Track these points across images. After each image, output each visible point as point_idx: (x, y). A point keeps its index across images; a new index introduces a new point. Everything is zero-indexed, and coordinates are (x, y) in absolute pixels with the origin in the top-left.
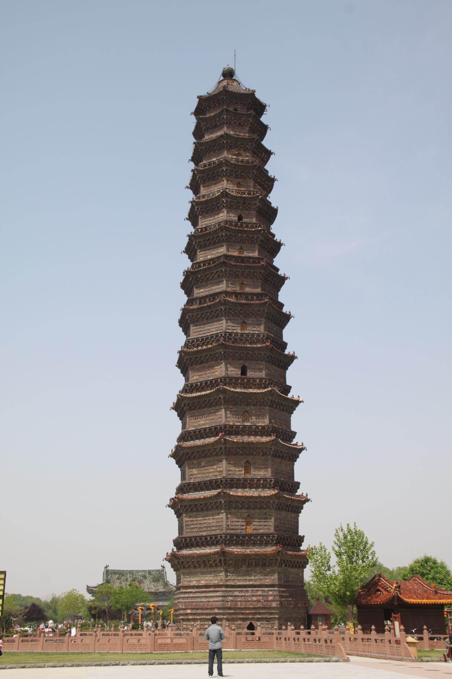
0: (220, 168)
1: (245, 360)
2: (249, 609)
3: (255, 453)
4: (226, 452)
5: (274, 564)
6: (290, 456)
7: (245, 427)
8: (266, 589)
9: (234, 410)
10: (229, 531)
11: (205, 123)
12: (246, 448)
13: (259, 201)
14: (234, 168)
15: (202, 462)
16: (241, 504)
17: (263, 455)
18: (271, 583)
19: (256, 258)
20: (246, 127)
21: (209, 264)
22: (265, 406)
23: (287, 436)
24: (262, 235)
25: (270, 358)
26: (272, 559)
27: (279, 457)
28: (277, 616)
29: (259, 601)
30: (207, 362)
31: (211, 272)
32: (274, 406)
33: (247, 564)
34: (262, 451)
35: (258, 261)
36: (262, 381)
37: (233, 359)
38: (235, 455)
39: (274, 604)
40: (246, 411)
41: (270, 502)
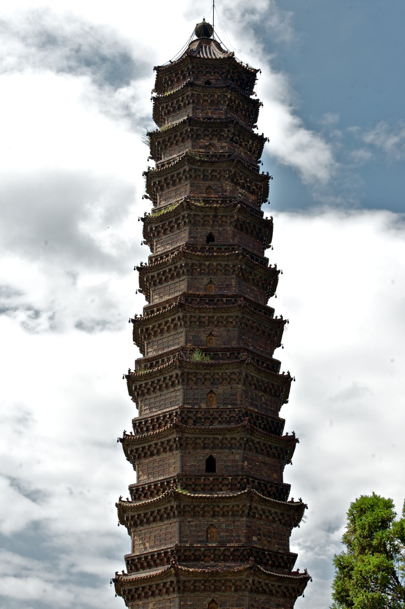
0: (181, 167)
1: (213, 448)
3: (223, 588)
4: (179, 588)
6: (285, 590)
9: (193, 524)
12: (210, 581)
15: (149, 603)
17: (236, 590)
20: (223, 105)
21: (164, 308)
22: (242, 516)
23: (281, 560)
25: (251, 444)
27: (264, 592)
31: (166, 320)
32: (257, 515)
35: (235, 300)
36: (236, 479)
37: (194, 448)
38: (194, 591)
40: (212, 525)
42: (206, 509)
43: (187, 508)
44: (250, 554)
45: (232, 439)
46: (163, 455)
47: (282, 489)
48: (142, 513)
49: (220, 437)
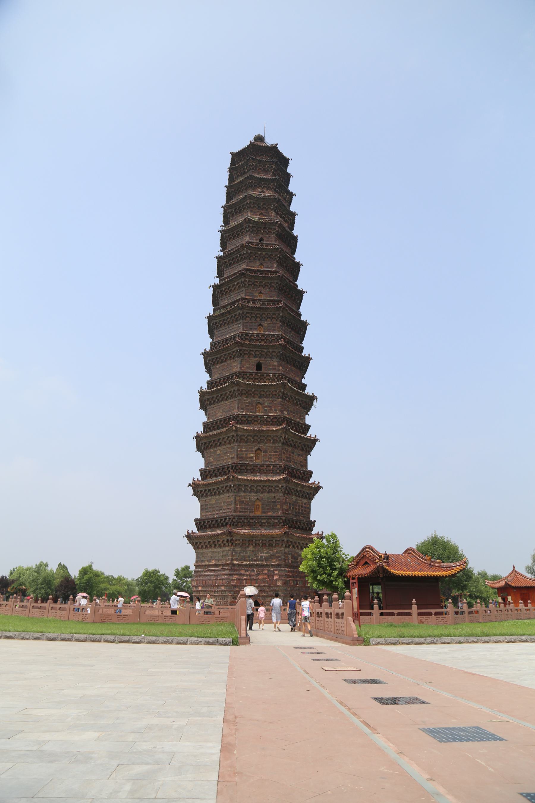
5: (280, 545)
10: (238, 514)
11: (235, 172)
13: (278, 227)
14: (256, 201)
24: (280, 253)
26: (279, 541)
27: (291, 445)
30: (225, 361)
33: (254, 545)
34: (272, 439)
36: (275, 376)
40: (259, 403)
41: (278, 487)
42: (256, 392)
43: (244, 392)
44: (283, 421)
45: (273, 352)
46: (230, 361)
47: (302, 387)
48: (215, 396)
49: (265, 351)
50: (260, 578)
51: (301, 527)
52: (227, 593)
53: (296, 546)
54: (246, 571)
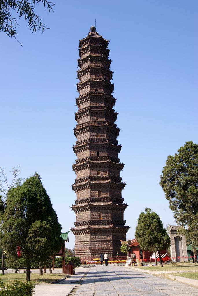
1: (99, 149)
2: (100, 250)
5: (110, 232)
7: (98, 177)
8: (107, 242)
10: (92, 220)
16: (97, 208)
18: (110, 239)
19: (103, 106)
27: (114, 188)
28: (112, 253)
29: (104, 247)
38: (94, 188)
39: (111, 248)
50: (103, 246)
51: (119, 223)
52: (89, 253)
53: (117, 232)
54: (97, 243)
